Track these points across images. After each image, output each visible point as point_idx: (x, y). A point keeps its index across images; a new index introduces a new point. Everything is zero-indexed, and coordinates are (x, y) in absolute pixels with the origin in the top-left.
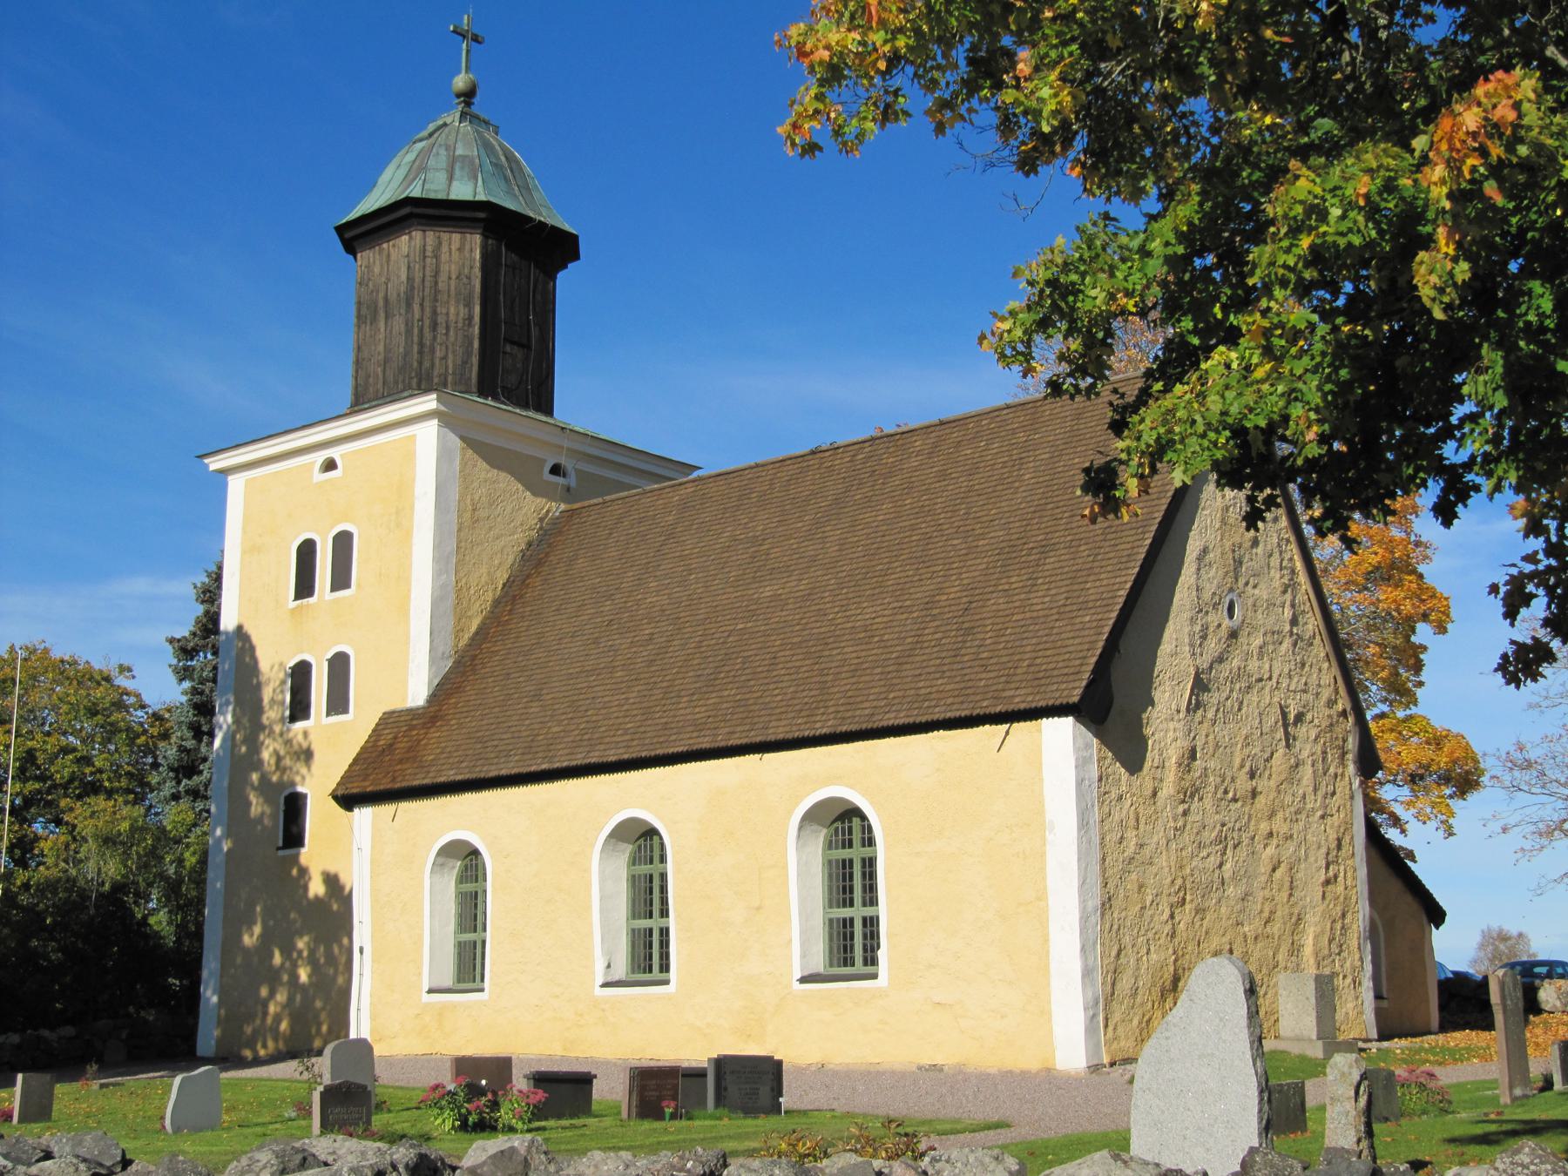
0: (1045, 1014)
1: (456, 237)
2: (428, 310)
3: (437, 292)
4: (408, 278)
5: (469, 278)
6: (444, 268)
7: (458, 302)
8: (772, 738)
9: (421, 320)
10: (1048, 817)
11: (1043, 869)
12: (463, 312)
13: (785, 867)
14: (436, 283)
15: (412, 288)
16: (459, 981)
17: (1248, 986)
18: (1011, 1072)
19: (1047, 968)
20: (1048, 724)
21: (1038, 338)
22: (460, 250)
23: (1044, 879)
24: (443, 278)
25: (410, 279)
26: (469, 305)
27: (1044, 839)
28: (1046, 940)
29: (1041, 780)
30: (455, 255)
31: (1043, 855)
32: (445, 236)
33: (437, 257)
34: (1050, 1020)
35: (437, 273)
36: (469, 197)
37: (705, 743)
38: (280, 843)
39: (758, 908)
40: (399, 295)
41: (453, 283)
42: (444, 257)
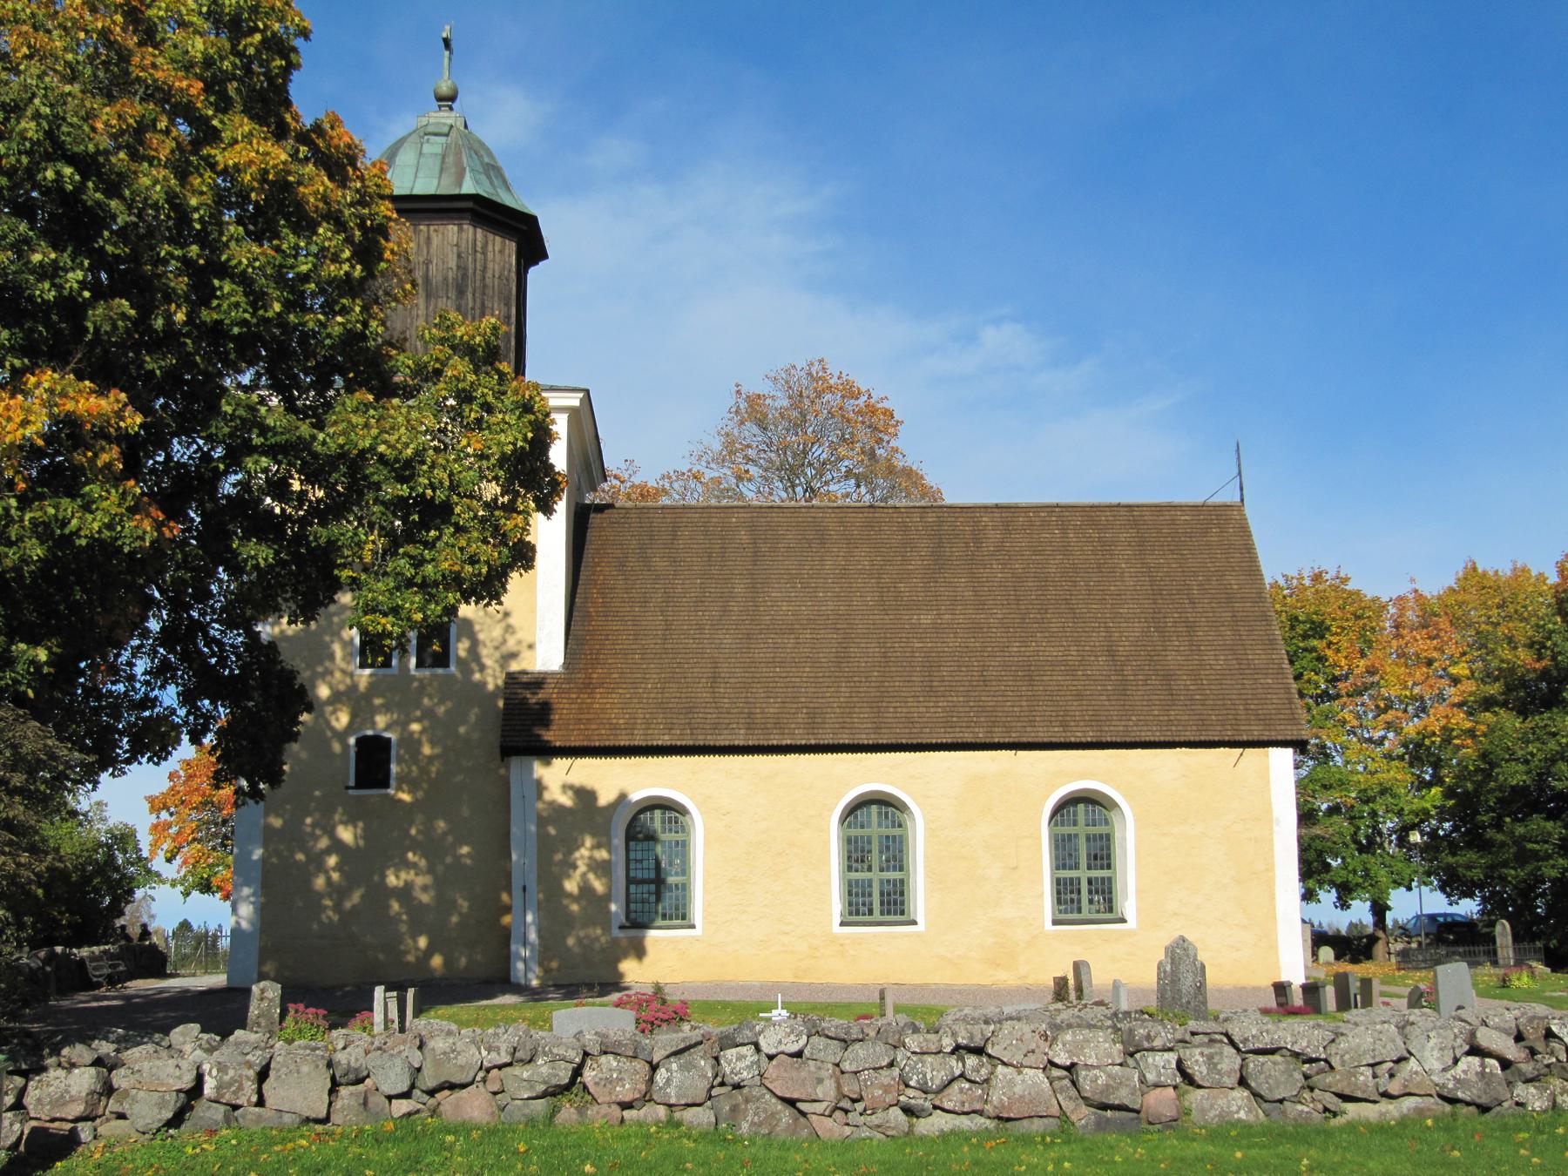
0: (1273, 947)
1: (498, 239)
2: (478, 301)
3: (485, 286)
4: (458, 267)
5: (507, 280)
6: (490, 265)
7: (500, 300)
8: (1025, 740)
9: (473, 309)
10: (1275, 815)
11: (1271, 850)
12: (504, 309)
13: (1039, 838)
14: (484, 278)
15: (465, 276)
16: (850, 914)
17: (674, 998)
18: (1244, 988)
19: (1274, 918)
20: (1274, 752)
21: (403, 366)
22: (501, 252)
23: (1273, 856)
24: (489, 274)
25: (461, 268)
26: (507, 305)
27: (1271, 830)
28: (1273, 898)
29: (1269, 790)
30: (498, 256)
31: (1271, 840)
32: (491, 236)
33: (484, 253)
34: (1277, 953)
35: (485, 269)
36: (431, 191)
37: (968, 738)
38: (352, 783)
39: (1015, 868)
40: (446, 279)
41: (496, 281)
42: (490, 255)
